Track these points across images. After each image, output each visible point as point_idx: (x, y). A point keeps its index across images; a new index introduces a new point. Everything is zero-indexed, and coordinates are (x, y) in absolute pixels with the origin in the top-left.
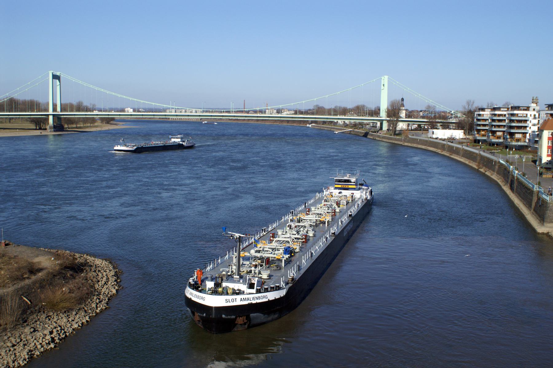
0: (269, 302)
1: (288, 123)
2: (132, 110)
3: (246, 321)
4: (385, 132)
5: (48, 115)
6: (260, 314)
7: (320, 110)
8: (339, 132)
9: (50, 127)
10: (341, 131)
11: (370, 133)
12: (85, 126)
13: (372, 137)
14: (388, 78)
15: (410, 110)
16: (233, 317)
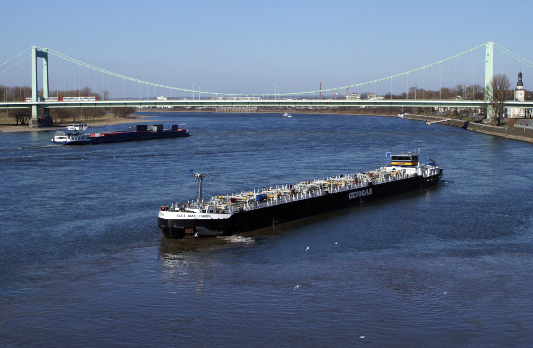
0: (212, 220)
1: (374, 113)
2: (166, 99)
3: (194, 232)
4: (490, 121)
5: (31, 105)
6: (205, 228)
7: (421, 94)
8: (432, 122)
9: (33, 121)
11: (470, 122)
12: (87, 120)
13: (471, 129)
14: (494, 45)
16: (182, 227)
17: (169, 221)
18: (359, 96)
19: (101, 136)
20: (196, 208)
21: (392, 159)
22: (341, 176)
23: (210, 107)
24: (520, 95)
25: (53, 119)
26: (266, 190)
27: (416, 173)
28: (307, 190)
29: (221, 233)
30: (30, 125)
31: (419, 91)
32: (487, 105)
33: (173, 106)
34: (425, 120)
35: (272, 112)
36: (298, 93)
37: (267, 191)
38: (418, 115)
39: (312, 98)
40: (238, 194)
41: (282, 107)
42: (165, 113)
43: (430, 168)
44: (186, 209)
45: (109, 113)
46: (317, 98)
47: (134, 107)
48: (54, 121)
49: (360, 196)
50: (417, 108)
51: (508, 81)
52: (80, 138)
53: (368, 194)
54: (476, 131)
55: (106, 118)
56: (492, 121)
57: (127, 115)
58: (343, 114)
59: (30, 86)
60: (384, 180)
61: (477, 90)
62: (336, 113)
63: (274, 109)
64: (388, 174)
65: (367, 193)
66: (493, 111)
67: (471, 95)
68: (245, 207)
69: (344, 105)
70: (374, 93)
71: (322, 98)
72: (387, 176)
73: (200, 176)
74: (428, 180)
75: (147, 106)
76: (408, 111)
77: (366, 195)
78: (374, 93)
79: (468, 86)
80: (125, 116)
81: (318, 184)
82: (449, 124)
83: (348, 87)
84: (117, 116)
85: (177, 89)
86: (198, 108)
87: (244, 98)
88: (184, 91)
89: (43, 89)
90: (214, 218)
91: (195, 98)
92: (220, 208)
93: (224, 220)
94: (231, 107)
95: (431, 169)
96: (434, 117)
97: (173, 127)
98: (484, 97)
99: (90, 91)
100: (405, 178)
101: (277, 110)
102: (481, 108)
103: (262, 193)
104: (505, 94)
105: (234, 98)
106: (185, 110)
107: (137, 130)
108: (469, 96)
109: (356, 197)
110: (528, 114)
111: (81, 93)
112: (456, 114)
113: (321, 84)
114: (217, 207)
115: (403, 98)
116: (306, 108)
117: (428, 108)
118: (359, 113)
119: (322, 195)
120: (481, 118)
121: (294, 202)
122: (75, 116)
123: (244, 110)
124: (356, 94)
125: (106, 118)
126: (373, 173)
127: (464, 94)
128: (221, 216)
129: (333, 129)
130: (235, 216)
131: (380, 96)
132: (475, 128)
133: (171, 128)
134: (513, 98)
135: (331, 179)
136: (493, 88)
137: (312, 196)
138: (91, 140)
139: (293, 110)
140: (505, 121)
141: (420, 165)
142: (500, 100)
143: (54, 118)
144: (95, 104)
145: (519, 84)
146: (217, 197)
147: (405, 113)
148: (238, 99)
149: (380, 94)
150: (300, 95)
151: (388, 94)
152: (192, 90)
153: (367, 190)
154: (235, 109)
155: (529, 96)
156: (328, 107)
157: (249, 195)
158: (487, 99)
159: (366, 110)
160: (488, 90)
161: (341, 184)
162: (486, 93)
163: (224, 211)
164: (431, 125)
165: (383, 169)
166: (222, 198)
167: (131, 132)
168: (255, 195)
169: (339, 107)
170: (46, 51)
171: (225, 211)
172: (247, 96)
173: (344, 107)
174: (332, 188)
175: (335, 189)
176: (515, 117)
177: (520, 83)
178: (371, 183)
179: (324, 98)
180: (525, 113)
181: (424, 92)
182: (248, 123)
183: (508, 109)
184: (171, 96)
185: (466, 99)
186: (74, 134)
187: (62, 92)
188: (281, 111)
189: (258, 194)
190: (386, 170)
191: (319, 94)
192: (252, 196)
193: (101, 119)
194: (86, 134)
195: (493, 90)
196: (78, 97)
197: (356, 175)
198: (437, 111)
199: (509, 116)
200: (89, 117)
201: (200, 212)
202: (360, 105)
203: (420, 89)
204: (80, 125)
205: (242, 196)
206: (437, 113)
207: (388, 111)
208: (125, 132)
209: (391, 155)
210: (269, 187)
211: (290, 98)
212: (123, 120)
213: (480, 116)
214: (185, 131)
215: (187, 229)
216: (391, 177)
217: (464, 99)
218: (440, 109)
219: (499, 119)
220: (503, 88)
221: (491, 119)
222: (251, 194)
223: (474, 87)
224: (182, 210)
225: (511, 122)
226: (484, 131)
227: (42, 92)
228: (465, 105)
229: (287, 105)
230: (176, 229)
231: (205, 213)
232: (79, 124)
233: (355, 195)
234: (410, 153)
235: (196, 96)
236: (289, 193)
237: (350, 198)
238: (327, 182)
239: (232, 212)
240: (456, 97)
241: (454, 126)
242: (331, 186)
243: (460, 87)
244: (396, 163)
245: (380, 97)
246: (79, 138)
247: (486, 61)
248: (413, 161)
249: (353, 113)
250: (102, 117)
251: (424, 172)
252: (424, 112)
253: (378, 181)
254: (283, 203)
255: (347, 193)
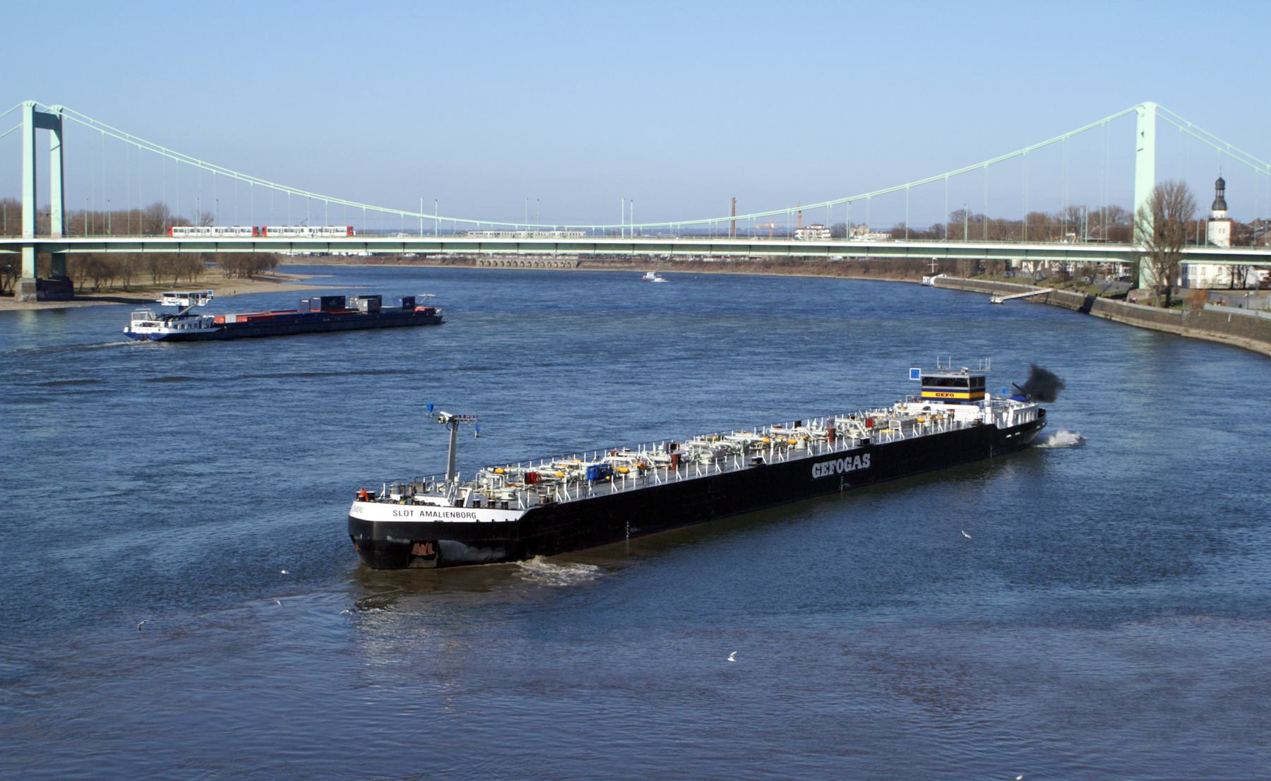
0: (478, 524)
1: (865, 272)
3: (433, 552)
5: (19, 246)
6: (460, 543)
7: (979, 228)
8: (1006, 297)
9: (24, 286)
10: (1013, 296)
12: (159, 285)
14: (1158, 109)
15: (1246, 220)
16: (406, 541)
17: (375, 526)
18: (827, 231)
19: (240, 321)
20: (437, 493)
21: (924, 384)
22: (798, 424)
23: (462, 256)
24: (1220, 233)
25: (74, 281)
26: (613, 455)
27: (979, 417)
28: (711, 455)
29: (500, 554)
30: (16, 295)
31: (975, 220)
32: (1139, 255)
33: (371, 251)
34: (988, 291)
35: (616, 267)
36: (678, 224)
37: (616, 458)
38: (970, 280)
39: (713, 236)
40: (544, 463)
41: (640, 255)
42: (353, 269)
43: (1015, 405)
44: (416, 497)
45: (213, 268)
46: (724, 235)
47: (276, 253)
48: (76, 285)
49: (839, 471)
50: (969, 262)
51: (1190, 197)
52: (193, 326)
53: (860, 467)
54: (1113, 319)
55: (205, 279)
56: (1151, 294)
57: (257, 273)
58: (788, 275)
59: (17, 199)
60: (901, 433)
61: (1116, 218)
62: (771, 273)
63: (621, 262)
64: (911, 421)
65: (857, 466)
66: (1155, 271)
67: (1101, 230)
68: (557, 494)
69: (792, 254)
70: (864, 224)
71: (737, 235)
72: (909, 424)
73: (451, 420)
74: (1009, 436)
75: (307, 252)
76: (947, 270)
77: (854, 468)
78: (864, 224)
79: (1093, 209)
80: (253, 275)
81: (739, 443)
82: (1046, 300)
83: (801, 208)
84: (234, 275)
85: (381, 209)
86: (433, 257)
87: (547, 233)
88: (399, 215)
89: (50, 206)
90: (482, 520)
91: (426, 233)
92: (500, 495)
93: (507, 523)
94: (515, 254)
95: (1016, 408)
96: (1010, 284)
97: (405, 300)
98: (1132, 236)
99: (167, 213)
100: (951, 430)
101: (626, 265)
102: (1124, 264)
103: (602, 462)
104: (1183, 230)
105: (522, 232)
106: (401, 261)
107: (322, 309)
108: (1096, 234)
109: (831, 473)
110: (1239, 279)
111: (143, 217)
112: (1064, 276)
113: (734, 201)
114: (492, 494)
115: (934, 238)
116: (698, 259)
117: (996, 262)
118: (829, 274)
119: (748, 468)
120: (1124, 286)
121: (678, 483)
122: (129, 274)
123: (546, 263)
124: (820, 227)
125: (205, 279)
126: (875, 417)
127: (1084, 228)
128: (499, 516)
129: (766, 312)
130: (532, 517)
131: (879, 233)
132: (1110, 312)
133: (401, 305)
134: (1202, 240)
135: (772, 430)
136: (1156, 215)
137: (722, 470)
138: (217, 331)
139: (666, 264)
140: (1182, 295)
141: (991, 399)
142: (1171, 245)
143: (78, 278)
144: (254, 245)
145: (1217, 206)
146: (492, 470)
147: (939, 274)
148: (531, 236)
149: (879, 227)
150: (683, 228)
151: (900, 227)
152: (419, 212)
153: (857, 458)
154: (525, 260)
155: (1240, 236)
156: (751, 258)
157: (571, 467)
158: (1139, 240)
159: (846, 266)
160: (1141, 220)
161: (794, 441)
162: (1138, 227)
163: (506, 503)
164: (1002, 303)
165: (899, 408)
166: (505, 473)
167: (307, 312)
168: (584, 467)
169: (779, 256)
170: (58, 114)
171: (510, 503)
172: (553, 230)
173: (792, 257)
174: (772, 450)
175: (780, 454)
176: (1206, 287)
177: (1221, 203)
178: (867, 441)
179: (742, 235)
180: (1230, 278)
181: (986, 224)
182: (550, 294)
183: (1189, 266)
184: (365, 228)
185: (1089, 241)
186: (177, 316)
187: (96, 213)
188: (637, 267)
189: (591, 464)
190: (907, 411)
191: (730, 226)
192: (577, 467)
193: (193, 281)
194: (205, 316)
195: (1155, 219)
196: (304, 228)
197: (832, 422)
198: (1018, 269)
199: (1191, 282)
200: (164, 276)
201: (448, 504)
202: (830, 254)
203: (977, 216)
204: (190, 295)
205: (553, 467)
206: (1018, 275)
207: (899, 268)
208: (295, 313)
209: (920, 375)
210: (620, 448)
211: (660, 233)
212: (248, 285)
213: (1122, 283)
214: (432, 311)
215: (416, 546)
216: (917, 426)
217: (1084, 241)
218: (1024, 264)
219: (1167, 291)
220: (1178, 214)
221: (1147, 290)
222: (576, 462)
223: (1107, 212)
224: (408, 499)
225: (1197, 297)
226: (1132, 319)
227: (48, 215)
228: (1085, 256)
229: (651, 253)
230: (391, 544)
231: (462, 506)
232: (188, 293)
233: (828, 469)
234: (966, 371)
235: (428, 228)
236: (667, 463)
237: (815, 476)
238: (762, 436)
239: (526, 507)
240: (1064, 235)
241: (1060, 306)
242: (770, 448)
243: (1073, 212)
244: (933, 395)
245: (878, 235)
246: (190, 325)
247: (1138, 148)
248: (974, 388)
249: (813, 273)
250: (195, 278)
251: (998, 416)
252: (987, 273)
253: (884, 435)
254: (651, 486)
255: (809, 463)
